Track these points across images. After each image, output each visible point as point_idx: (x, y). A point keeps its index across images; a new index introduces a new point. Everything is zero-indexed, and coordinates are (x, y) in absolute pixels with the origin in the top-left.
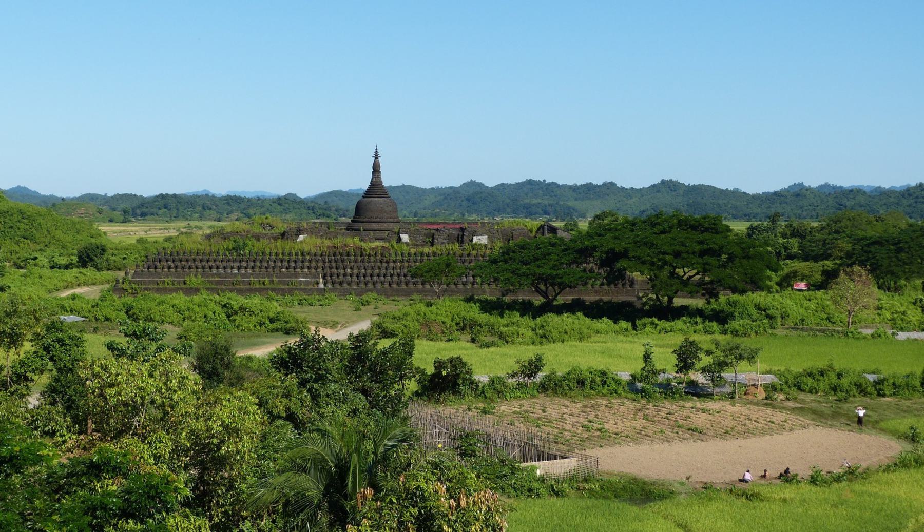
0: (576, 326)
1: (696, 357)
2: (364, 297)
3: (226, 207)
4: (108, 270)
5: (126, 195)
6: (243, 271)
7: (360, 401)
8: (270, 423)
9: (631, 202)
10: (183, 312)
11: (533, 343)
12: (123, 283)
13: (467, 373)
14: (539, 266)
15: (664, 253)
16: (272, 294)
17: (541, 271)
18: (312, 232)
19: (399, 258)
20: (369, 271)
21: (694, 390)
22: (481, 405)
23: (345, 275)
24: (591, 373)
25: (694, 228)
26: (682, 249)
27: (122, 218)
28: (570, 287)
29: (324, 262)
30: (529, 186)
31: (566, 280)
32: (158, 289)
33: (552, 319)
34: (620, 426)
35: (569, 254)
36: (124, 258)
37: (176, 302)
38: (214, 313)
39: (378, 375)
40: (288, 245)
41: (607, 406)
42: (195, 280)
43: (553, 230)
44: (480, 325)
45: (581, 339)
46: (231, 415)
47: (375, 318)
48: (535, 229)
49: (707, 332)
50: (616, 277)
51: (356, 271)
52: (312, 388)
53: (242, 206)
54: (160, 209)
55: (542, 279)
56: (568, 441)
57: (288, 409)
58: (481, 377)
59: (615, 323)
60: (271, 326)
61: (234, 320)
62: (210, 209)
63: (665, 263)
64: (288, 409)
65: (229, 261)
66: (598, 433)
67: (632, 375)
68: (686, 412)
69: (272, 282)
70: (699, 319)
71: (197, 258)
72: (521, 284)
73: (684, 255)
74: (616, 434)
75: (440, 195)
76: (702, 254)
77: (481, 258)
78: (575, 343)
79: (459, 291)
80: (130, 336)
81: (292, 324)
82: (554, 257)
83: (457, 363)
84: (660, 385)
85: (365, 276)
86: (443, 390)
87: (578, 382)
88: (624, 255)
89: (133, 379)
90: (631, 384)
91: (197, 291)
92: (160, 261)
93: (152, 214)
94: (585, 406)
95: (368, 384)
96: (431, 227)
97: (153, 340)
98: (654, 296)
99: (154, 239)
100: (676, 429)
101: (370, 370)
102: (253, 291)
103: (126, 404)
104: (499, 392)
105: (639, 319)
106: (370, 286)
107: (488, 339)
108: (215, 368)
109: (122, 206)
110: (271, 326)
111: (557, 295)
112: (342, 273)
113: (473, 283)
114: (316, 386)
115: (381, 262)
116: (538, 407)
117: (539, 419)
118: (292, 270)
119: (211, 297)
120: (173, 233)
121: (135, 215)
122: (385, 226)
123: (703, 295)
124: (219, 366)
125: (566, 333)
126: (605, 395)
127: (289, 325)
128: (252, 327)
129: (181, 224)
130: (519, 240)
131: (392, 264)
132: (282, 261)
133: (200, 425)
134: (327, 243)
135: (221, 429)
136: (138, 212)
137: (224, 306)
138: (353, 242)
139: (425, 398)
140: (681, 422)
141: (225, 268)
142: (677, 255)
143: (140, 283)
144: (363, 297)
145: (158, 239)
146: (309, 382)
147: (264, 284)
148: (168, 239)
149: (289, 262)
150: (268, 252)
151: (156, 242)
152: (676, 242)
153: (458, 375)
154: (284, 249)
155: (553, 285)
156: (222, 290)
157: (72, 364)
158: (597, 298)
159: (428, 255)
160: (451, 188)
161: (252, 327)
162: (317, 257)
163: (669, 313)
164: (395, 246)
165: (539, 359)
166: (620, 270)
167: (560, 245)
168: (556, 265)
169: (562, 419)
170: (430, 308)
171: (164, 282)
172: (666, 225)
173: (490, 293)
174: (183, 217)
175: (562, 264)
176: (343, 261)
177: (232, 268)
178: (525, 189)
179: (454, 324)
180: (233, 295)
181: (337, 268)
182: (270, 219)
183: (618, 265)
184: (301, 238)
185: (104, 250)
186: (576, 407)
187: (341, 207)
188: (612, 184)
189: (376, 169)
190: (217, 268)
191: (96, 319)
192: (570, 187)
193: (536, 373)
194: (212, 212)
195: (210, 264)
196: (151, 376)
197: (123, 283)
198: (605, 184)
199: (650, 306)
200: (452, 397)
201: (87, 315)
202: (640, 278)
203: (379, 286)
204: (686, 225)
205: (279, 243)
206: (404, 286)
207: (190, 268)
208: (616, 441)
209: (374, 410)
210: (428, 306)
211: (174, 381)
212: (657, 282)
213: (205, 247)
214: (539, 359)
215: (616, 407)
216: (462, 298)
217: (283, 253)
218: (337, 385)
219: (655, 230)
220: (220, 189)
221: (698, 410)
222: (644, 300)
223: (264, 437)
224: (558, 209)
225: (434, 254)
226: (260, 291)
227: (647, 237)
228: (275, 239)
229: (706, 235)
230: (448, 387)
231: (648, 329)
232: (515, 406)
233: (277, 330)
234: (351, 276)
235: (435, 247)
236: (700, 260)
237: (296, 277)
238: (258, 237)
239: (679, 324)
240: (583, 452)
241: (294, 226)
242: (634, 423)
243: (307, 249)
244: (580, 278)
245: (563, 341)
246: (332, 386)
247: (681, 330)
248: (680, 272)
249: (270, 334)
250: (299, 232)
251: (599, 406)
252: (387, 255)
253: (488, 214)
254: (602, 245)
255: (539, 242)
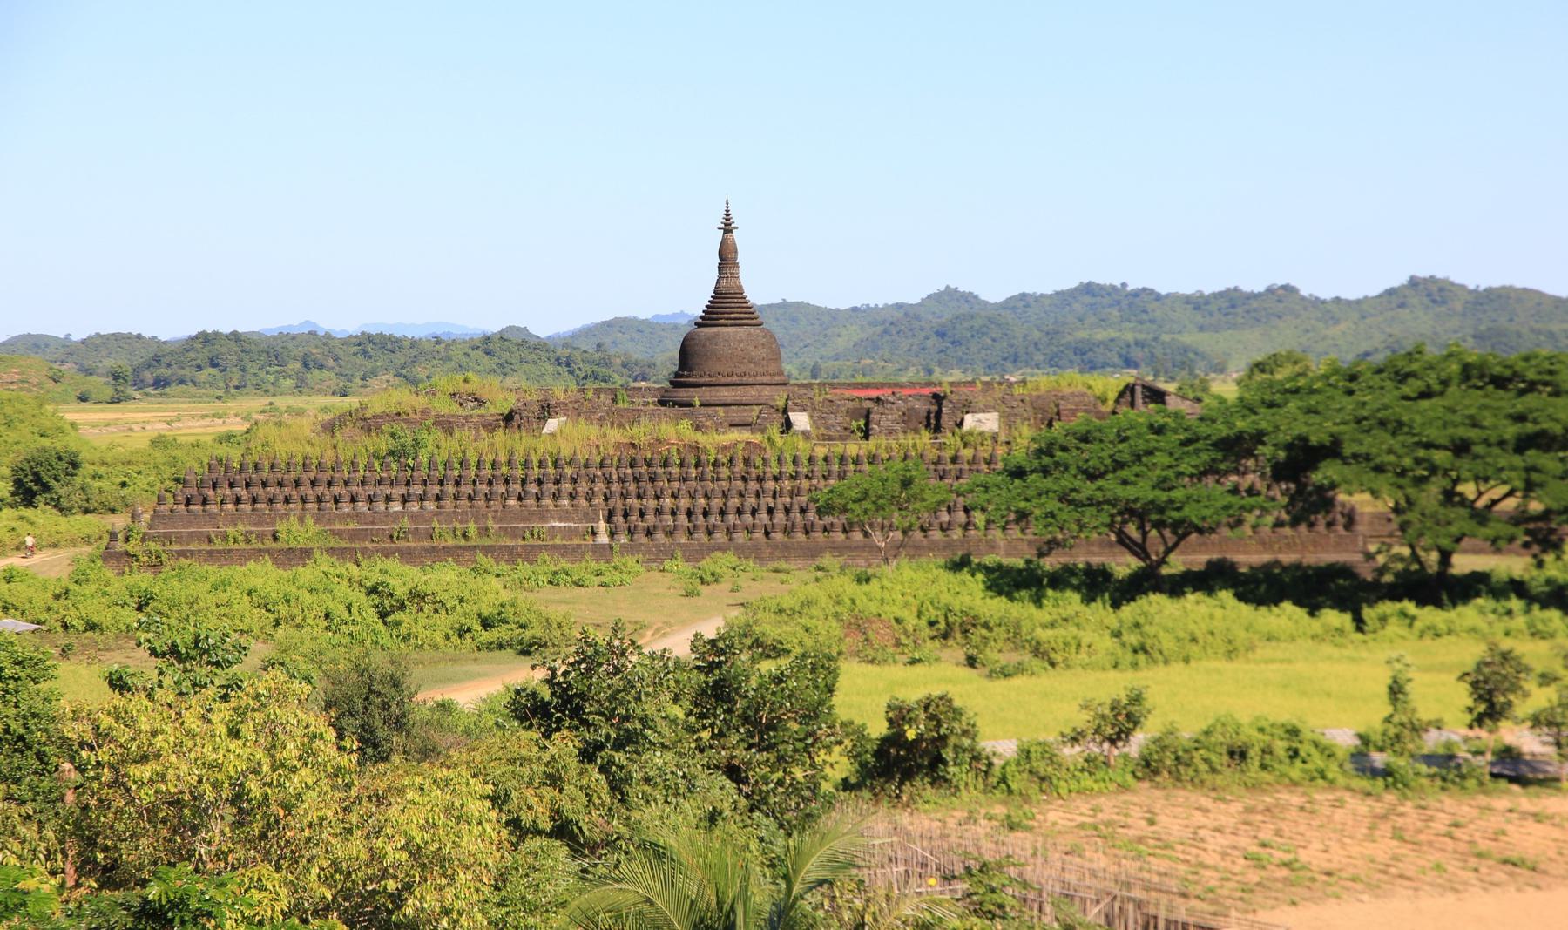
0: (1218, 625)
1: (1515, 688)
2: (707, 564)
3: (359, 360)
4: (87, 511)
5: (116, 337)
6: (415, 507)
7: (722, 792)
8: (515, 846)
9: (1334, 331)
10: (290, 604)
11: (1115, 666)
12: (127, 540)
13: (965, 733)
14: (1125, 482)
15: (1429, 446)
16: (485, 561)
17: (1130, 492)
18: (576, 411)
19: (789, 468)
20: (717, 502)
21: (1513, 769)
22: (1000, 811)
23: (658, 512)
24: (1261, 730)
25: (1500, 382)
26: (1473, 434)
27: (109, 392)
28: (1200, 531)
29: (608, 481)
30: (1088, 299)
31: (1191, 513)
32: (210, 553)
33: (1155, 604)
34: (1337, 858)
35: (1197, 452)
36: (124, 484)
37: (256, 582)
38: (349, 608)
39: (762, 731)
40: (520, 443)
41: (1302, 809)
42: (298, 529)
43: (1157, 396)
44: (986, 626)
45: (1231, 654)
46: (430, 825)
47: (735, 614)
48: (1112, 396)
49: (1535, 634)
50: (1311, 506)
51: (684, 503)
52: (611, 762)
53: (399, 359)
54: (200, 368)
55: (1132, 512)
56: (1211, 890)
57: (556, 813)
58: (1001, 746)
59: (1312, 614)
60: (486, 636)
61: (398, 624)
62: (321, 367)
63: (1433, 469)
64: (556, 813)
65: (380, 482)
66: (1285, 872)
67: (1360, 736)
68: (1495, 822)
69: (484, 532)
70: (1516, 604)
71: (304, 477)
72: (1082, 527)
73: (1478, 449)
74: (1329, 874)
75: (873, 324)
76: (1523, 444)
77: (984, 467)
78: (1214, 664)
79: (933, 547)
80: (164, 655)
81: (536, 631)
82: (1161, 459)
83: (938, 709)
84: (1429, 759)
85: (706, 514)
86: (908, 775)
87: (1231, 754)
88: (1332, 450)
89: (188, 745)
90: (1360, 761)
91: (305, 554)
92: (214, 486)
93: (182, 382)
94: (1250, 810)
95: (741, 754)
96: (863, 394)
97: (217, 664)
98: (1406, 551)
99: (192, 439)
100: (1473, 862)
101: (746, 720)
102: (439, 554)
103: (176, 803)
104: (1043, 779)
105: (1371, 604)
106: (720, 537)
107: (1008, 658)
108: (373, 718)
109: (109, 363)
110: (486, 636)
111: (1168, 551)
112: (643, 505)
113: (966, 527)
114: (619, 757)
115: (744, 479)
116: (1136, 813)
117: (1140, 840)
118: (531, 502)
119: (340, 570)
120: (237, 426)
121: (139, 384)
122: (750, 394)
123: (1526, 545)
124: (378, 723)
125: (1194, 640)
126: (1295, 784)
127: (528, 634)
128: (440, 640)
129: (253, 404)
130: (1078, 422)
131: (770, 485)
132: (507, 481)
133: (356, 848)
134: (615, 435)
135: (404, 856)
136: (148, 376)
137: (373, 590)
138: (675, 431)
139: (866, 794)
140: (1484, 845)
141: (371, 500)
142: (1461, 448)
143: (168, 538)
144: (703, 563)
145: (203, 439)
146: (601, 747)
147: (464, 536)
148: (227, 438)
149: (524, 482)
150: (473, 460)
151: (196, 445)
152: (1457, 418)
153: (943, 739)
154: (512, 452)
155: (1159, 525)
156: (364, 551)
157: (25, 726)
158: (1266, 558)
159: (857, 462)
160: (899, 306)
161: (440, 640)
162: (592, 471)
163: (1436, 588)
164: (777, 438)
165: (1137, 699)
166: (1320, 489)
167: (1175, 431)
168: (1165, 479)
169: (1196, 840)
170: (865, 587)
171: (225, 537)
172: (1432, 379)
173: (1010, 550)
174: (257, 386)
175: (1180, 474)
176: (652, 479)
177: (388, 499)
178: (1076, 306)
179: (923, 622)
180: (393, 564)
181: (639, 496)
182: (476, 383)
183: (1316, 477)
184: (552, 424)
185: (75, 465)
186: (1228, 812)
187: (637, 356)
188: (1289, 290)
189: (727, 258)
190: (353, 500)
191: (66, 627)
192: (1188, 300)
193: (1128, 733)
194: (325, 373)
195: (336, 490)
196: (234, 734)
197: (127, 540)
198: (1270, 291)
199: (1397, 575)
200: (929, 792)
201: (43, 616)
202: (1368, 509)
203: (740, 537)
204: (1481, 377)
205: (500, 437)
206: (800, 536)
207: (287, 500)
208: (1330, 890)
209: (757, 814)
210: (859, 581)
211: (290, 746)
212: (1412, 516)
213: (320, 449)
214: (1137, 699)
215: (1326, 810)
216: (941, 561)
217: (509, 462)
218: (669, 756)
219: (1406, 390)
220: (343, 321)
221: (1525, 815)
222: (1381, 559)
223: (501, 880)
224: (1158, 352)
225: (872, 459)
226: (455, 553)
227: (1386, 407)
228: (490, 428)
229: (1531, 400)
230: (920, 767)
231: (1394, 628)
232: (1080, 811)
233: (500, 647)
234: (673, 513)
235: (872, 442)
236: (1517, 460)
237: (543, 519)
238: (447, 425)
239: (1470, 614)
240: (1250, 917)
241: (535, 397)
242: (1369, 849)
243: (566, 452)
244: (1226, 508)
245: (1187, 660)
246: (658, 758)
247: (1473, 630)
248: (1468, 489)
249: (484, 653)
250: (547, 410)
251: (1285, 807)
252: (759, 462)
253: (990, 368)
254: (1277, 428)
255: (1124, 424)
